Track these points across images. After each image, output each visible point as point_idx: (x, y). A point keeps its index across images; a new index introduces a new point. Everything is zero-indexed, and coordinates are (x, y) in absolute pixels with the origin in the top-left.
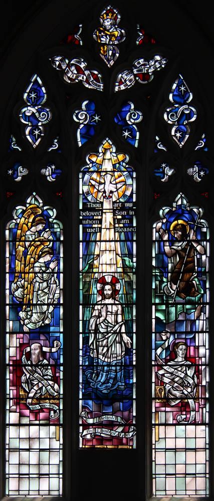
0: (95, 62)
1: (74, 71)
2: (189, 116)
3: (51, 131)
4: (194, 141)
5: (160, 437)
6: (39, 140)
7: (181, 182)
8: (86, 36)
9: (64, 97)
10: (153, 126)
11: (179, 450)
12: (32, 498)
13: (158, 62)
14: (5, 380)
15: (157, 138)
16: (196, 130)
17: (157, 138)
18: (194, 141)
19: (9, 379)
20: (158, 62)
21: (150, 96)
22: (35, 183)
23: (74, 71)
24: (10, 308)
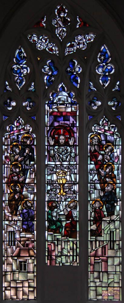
0: (53, 38)
1: (42, 44)
2: (110, 71)
3: (30, 78)
4: (112, 85)
5: (97, 283)
6: (102, 84)
7: (104, 110)
8: (49, 22)
9: (36, 58)
10: (89, 75)
11: (104, 285)
12: (6, 187)
13: (91, 37)
14: (2, 249)
15: (7, 83)
16: (115, 78)
17: (7, 83)
18: (112, 85)
19: (4, 249)
20: (91, 37)
21: (87, 57)
22: (19, 111)
23: (42, 44)
24: (5, 192)
